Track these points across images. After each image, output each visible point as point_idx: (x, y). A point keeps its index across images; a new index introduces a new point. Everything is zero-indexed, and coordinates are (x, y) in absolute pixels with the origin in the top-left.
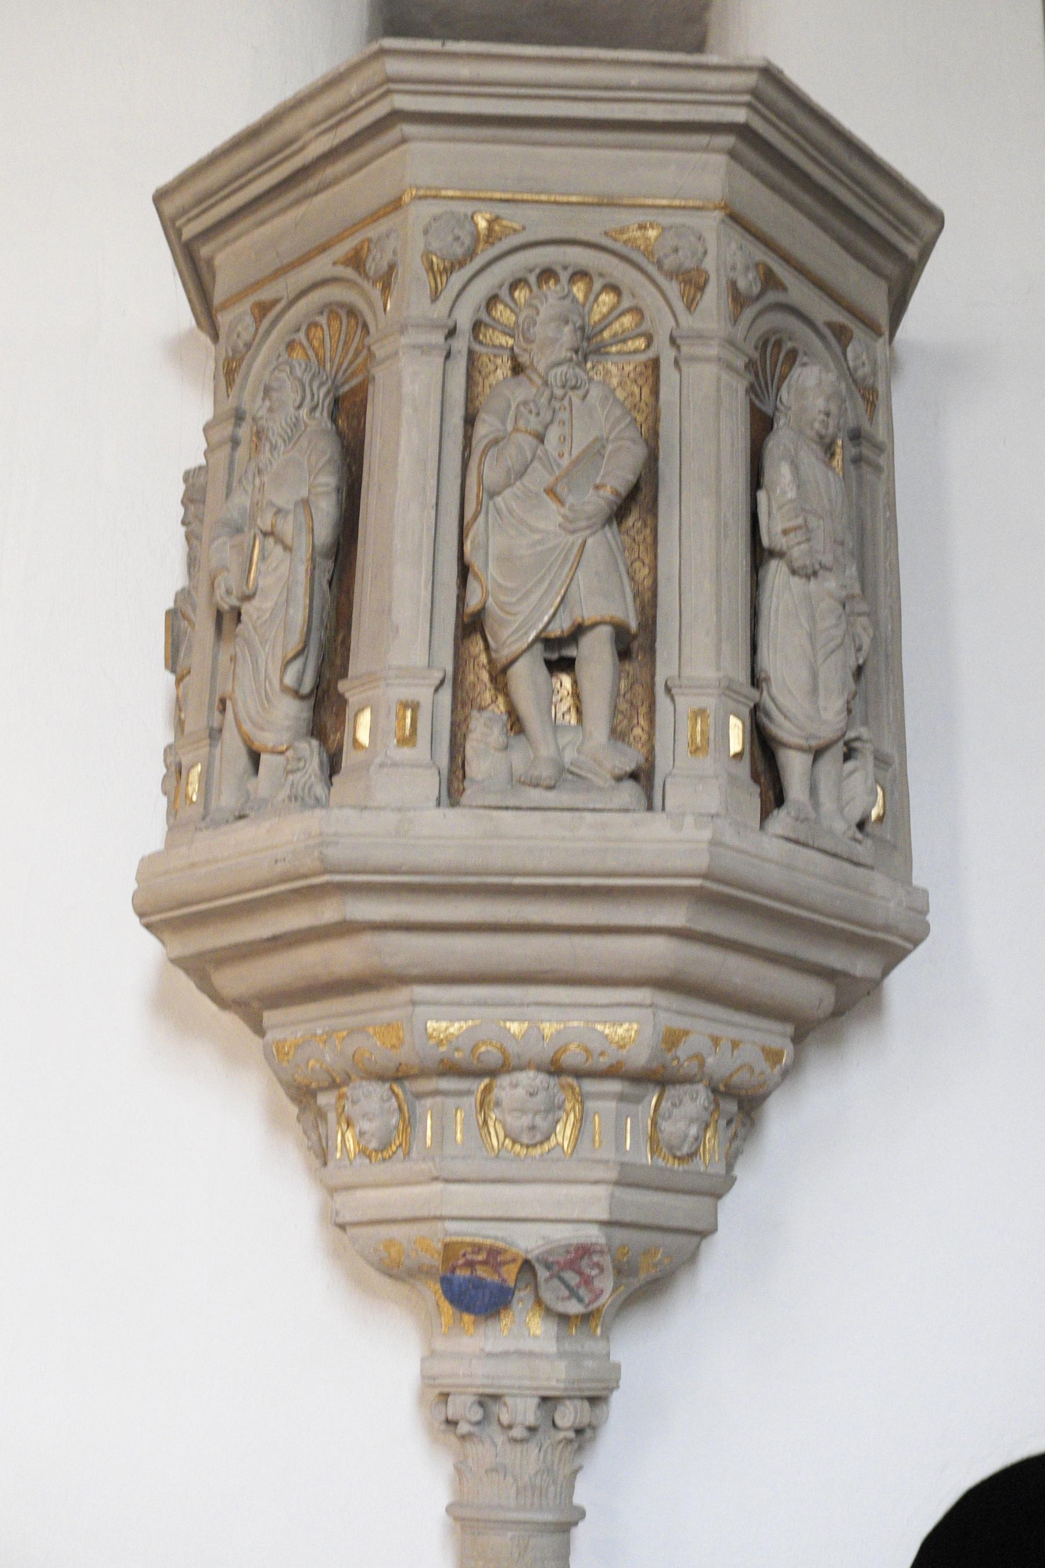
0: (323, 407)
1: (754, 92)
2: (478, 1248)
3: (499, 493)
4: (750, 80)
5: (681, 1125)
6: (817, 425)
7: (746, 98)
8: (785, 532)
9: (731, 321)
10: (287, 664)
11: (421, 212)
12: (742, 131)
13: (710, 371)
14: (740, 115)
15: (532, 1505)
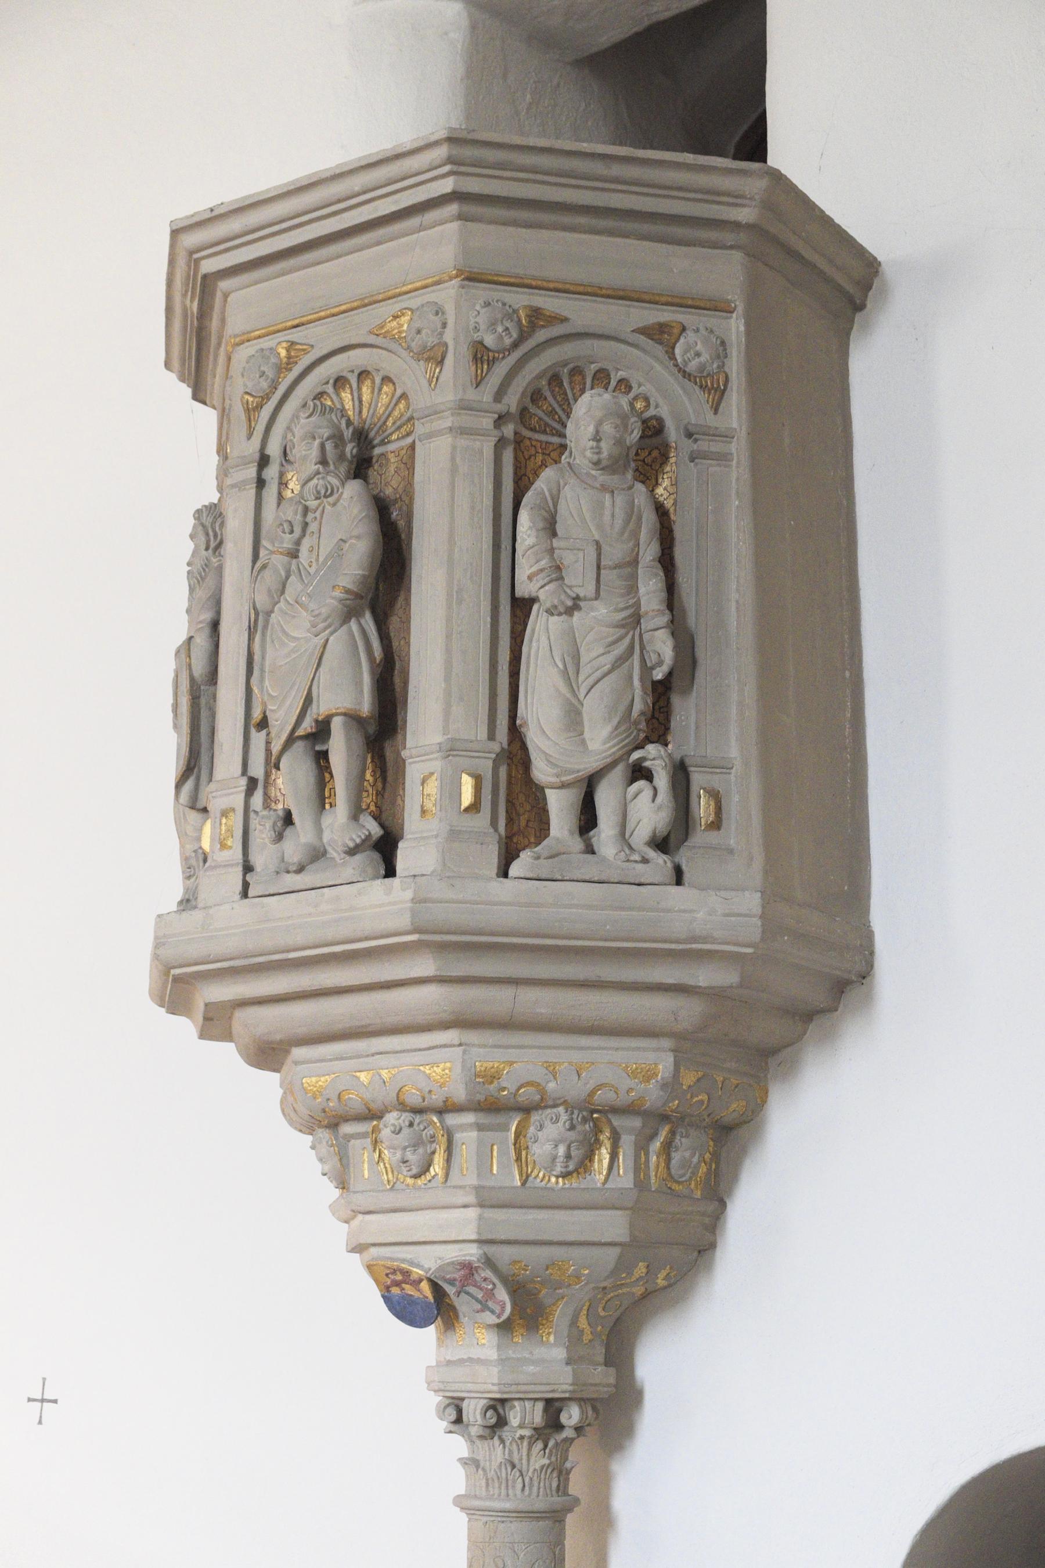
1: (450, 160)
3: (272, 611)
4: (441, 152)
6: (588, 454)
7: (447, 168)
8: (530, 578)
9: (472, 385)
12: (455, 196)
14: (447, 186)
15: (500, 1495)
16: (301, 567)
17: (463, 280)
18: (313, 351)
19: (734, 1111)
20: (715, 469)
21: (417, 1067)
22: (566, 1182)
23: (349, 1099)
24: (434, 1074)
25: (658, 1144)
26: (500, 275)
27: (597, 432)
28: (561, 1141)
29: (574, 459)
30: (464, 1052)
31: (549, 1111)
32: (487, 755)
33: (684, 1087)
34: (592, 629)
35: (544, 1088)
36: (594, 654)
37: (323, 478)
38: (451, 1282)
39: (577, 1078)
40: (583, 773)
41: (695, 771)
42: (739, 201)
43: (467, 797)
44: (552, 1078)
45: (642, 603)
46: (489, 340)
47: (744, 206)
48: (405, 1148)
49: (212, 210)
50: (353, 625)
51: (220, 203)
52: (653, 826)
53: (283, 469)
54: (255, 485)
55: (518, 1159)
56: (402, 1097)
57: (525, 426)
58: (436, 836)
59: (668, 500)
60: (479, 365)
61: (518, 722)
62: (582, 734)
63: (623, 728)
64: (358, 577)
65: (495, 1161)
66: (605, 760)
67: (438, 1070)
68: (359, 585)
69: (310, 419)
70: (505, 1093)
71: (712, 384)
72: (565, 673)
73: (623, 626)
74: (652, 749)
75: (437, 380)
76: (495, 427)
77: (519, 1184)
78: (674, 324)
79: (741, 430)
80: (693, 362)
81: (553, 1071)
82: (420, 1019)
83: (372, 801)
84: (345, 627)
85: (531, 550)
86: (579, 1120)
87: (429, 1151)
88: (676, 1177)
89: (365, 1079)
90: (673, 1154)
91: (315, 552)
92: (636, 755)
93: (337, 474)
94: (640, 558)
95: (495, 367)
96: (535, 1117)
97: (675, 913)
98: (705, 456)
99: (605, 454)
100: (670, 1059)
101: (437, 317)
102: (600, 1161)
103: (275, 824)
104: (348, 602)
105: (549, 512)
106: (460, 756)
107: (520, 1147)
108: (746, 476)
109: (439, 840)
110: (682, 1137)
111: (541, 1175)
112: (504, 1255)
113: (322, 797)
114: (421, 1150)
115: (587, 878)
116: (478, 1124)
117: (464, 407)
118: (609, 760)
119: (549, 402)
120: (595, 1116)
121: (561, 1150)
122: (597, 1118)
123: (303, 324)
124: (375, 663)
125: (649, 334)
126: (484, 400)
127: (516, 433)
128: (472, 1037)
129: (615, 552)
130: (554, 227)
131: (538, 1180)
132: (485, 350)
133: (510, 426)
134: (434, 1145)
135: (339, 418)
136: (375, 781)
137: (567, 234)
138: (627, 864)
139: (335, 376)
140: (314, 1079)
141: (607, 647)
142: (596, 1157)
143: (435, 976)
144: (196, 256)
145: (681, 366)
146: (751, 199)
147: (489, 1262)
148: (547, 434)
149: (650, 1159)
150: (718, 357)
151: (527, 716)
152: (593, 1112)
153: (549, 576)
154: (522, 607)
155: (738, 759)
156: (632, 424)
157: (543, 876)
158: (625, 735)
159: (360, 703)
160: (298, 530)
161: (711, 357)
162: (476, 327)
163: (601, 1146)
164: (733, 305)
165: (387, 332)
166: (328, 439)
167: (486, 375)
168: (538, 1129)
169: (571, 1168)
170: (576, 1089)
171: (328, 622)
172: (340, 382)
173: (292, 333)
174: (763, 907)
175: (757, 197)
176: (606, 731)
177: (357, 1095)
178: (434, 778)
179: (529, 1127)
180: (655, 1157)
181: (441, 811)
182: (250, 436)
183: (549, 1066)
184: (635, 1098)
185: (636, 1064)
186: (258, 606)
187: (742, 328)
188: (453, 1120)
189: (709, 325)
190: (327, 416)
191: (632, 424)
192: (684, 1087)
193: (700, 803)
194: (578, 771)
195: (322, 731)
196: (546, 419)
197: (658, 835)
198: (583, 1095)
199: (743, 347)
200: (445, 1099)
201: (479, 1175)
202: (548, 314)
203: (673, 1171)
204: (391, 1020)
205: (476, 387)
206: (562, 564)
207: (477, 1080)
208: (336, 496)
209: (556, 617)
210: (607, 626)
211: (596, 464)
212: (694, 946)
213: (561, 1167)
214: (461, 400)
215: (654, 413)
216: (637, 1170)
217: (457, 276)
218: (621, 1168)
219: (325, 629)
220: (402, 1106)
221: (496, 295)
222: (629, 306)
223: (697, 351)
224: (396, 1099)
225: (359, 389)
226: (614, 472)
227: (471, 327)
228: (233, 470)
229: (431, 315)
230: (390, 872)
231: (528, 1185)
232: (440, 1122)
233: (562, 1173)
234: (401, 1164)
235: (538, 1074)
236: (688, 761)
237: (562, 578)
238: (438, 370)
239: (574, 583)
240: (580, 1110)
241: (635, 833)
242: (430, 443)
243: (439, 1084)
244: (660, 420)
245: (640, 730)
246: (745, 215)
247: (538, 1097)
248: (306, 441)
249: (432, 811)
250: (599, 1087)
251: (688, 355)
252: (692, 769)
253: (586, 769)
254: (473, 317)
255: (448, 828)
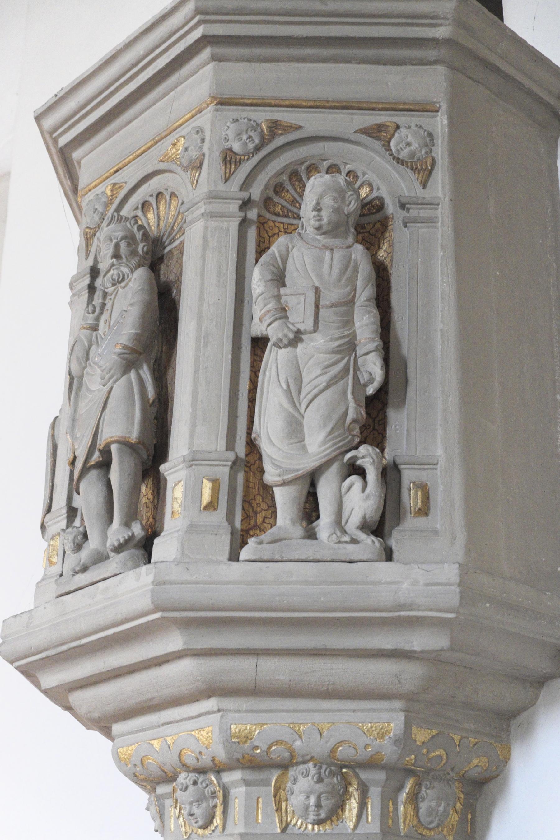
6: (312, 222)
16: (99, 336)
17: (216, 104)
18: (127, 186)
19: (477, 766)
20: (424, 230)
21: (190, 733)
22: (321, 829)
23: (149, 763)
24: (201, 737)
25: (404, 795)
26: (246, 98)
27: (318, 203)
28: (311, 792)
29: (306, 230)
30: (222, 717)
31: (301, 767)
32: (225, 463)
33: (418, 743)
34: (313, 356)
35: (291, 746)
36: (313, 376)
37: (117, 269)
39: (319, 736)
40: (302, 471)
41: (405, 469)
42: (435, 21)
43: (206, 497)
44: (298, 737)
45: (358, 333)
46: (237, 147)
47: (440, 25)
48: (191, 803)
49: (56, 96)
50: (133, 374)
51: (60, 89)
52: (363, 514)
54: (87, 291)
56: (183, 759)
57: (269, 212)
58: (178, 531)
59: (387, 259)
60: (228, 166)
61: (253, 436)
62: (303, 441)
63: (337, 434)
64: (132, 335)
65: (260, 811)
66: (321, 460)
67: (204, 733)
68: (133, 342)
69: (109, 227)
70: (258, 751)
71: (421, 166)
72: (288, 391)
73: (337, 352)
74: (364, 449)
75: (197, 181)
76: (239, 211)
77: (279, 831)
78: (389, 124)
79: (445, 198)
80: (405, 151)
81: (298, 731)
83: (151, 514)
84: (124, 378)
85: (260, 298)
86: (327, 773)
87: (211, 806)
88: (425, 824)
89: (157, 746)
90: (421, 804)
91: (108, 323)
93: (127, 265)
94: (356, 299)
95: (241, 166)
96: (292, 772)
97: (383, 585)
98: (415, 221)
99: (325, 220)
100: (401, 718)
101: (199, 135)
102: (351, 810)
103: (75, 537)
104: (125, 356)
105: (278, 268)
106: (202, 465)
107: (280, 798)
108: (450, 232)
109: (180, 533)
110: (427, 788)
111: (299, 823)
114: (204, 805)
115: (303, 557)
116: (244, 780)
117: (213, 197)
118: (324, 460)
119: (290, 194)
120: (344, 770)
121: (313, 800)
122: (345, 773)
123: (121, 169)
124: (149, 402)
125: (368, 133)
126: (232, 190)
127: (259, 216)
128: (229, 703)
130: (289, 59)
131: (297, 827)
132: (233, 155)
133: (254, 210)
134: (215, 800)
135: (132, 225)
136: (154, 498)
137: (301, 65)
138: (340, 545)
139: (141, 202)
140: (125, 749)
141: (324, 369)
142: (347, 806)
143: (184, 650)
144: (54, 136)
145: (395, 154)
146: (445, 18)
148: (290, 218)
149: (399, 808)
150: (426, 145)
151: (260, 432)
152: (342, 767)
153: (274, 315)
155: (443, 456)
156: (349, 197)
157: (265, 558)
158: (339, 439)
159: (130, 432)
161: (420, 146)
162: (226, 138)
163: (350, 797)
164: (438, 105)
166: (122, 239)
167: (234, 172)
168: (293, 783)
169: (323, 816)
171: (111, 373)
172: (145, 205)
173: (115, 178)
174: (461, 575)
175: (449, 16)
176: (322, 435)
177: (153, 760)
178: (180, 484)
179: (287, 781)
180: (402, 806)
181: (184, 510)
182: (87, 258)
183: (295, 727)
184: (373, 753)
185: (371, 723)
186: (73, 372)
187: (445, 122)
188: (228, 777)
189: (419, 124)
190: (123, 223)
191: (349, 197)
192: (418, 743)
193: (410, 495)
194: (298, 470)
196: (288, 206)
197: (368, 520)
198: (326, 750)
199: (446, 135)
200: (212, 759)
201: (246, 824)
202: (285, 125)
203: (422, 819)
204: (166, 693)
205: (226, 182)
206: (287, 306)
207: (233, 740)
209: (283, 350)
210: (324, 353)
211: (319, 228)
212: (402, 613)
213: (314, 815)
214: (211, 192)
215: (376, 195)
216: (384, 815)
217: (212, 102)
218: (370, 816)
219: (110, 379)
221: (245, 114)
222: (352, 114)
223: (408, 142)
224: (179, 761)
225: (158, 208)
226: (336, 236)
227: (223, 138)
228: (76, 283)
229: (194, 135)
231: (288, 832)
232: (217, 780)
233: (314, 820)
234: (190, 817)
235: (285, 734)
236: (398, 461)
237: (286, 317)
238: (197, 174)
239: (297, 320)
240: (329, 765)
241: (350, 520)
242: (191, 229)
243: (205, 746)
244: (381, 200)
245: (354, 436)
247: (287, 754)
248: (106, 244)
249: (178, 511)
250: (340, 744)
251: (401, 145)
252: (402, 467)
253: (304, 468)
254: (224, 131)
255: (189, 523)
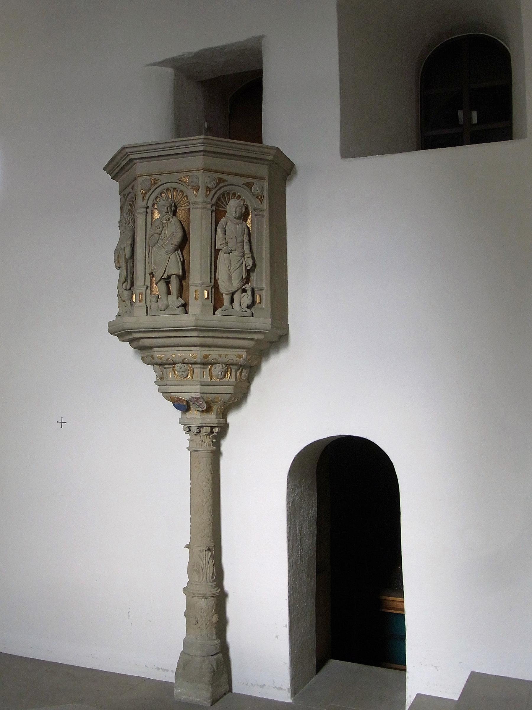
0: (131, 223)
2: (177, 398)
5: (217, 372)
10: (122, 285)
11: (140, 180)
13: (199, 211)
14: (202, 148)
15: (200, 447)
38: (192, 401)
43: (206, 296)
53: (152, 210)
55: (210, 375)
77: (210, 380)
82: (191, 345)
92: (243, 287)
96: (214, 366)
98: (259, 215)
99: (237, 215)
109: (200, 306)
112: (205, 396)
113: (169, 293)
114: (186, 372)
117: (204, 202)
121: (220, 373)
129: (239, 239)
147: (202, 398)
154: (217, 251)
159: (179, 272)
160: (161, 229)
165: (183, 180)
170: (225, 360)
172: (168, 190)
176: (238, 282)
187: (267, 184)
195: (169, 277)
204: (182, 344)
208: (171, 220)
211: (235, 218)
217: (202, 170)
220: (183, 362)
225: (173, 192)
230: (187, 313)
235: (217, 357)
238: (197, 192)
246: (270, 158)
